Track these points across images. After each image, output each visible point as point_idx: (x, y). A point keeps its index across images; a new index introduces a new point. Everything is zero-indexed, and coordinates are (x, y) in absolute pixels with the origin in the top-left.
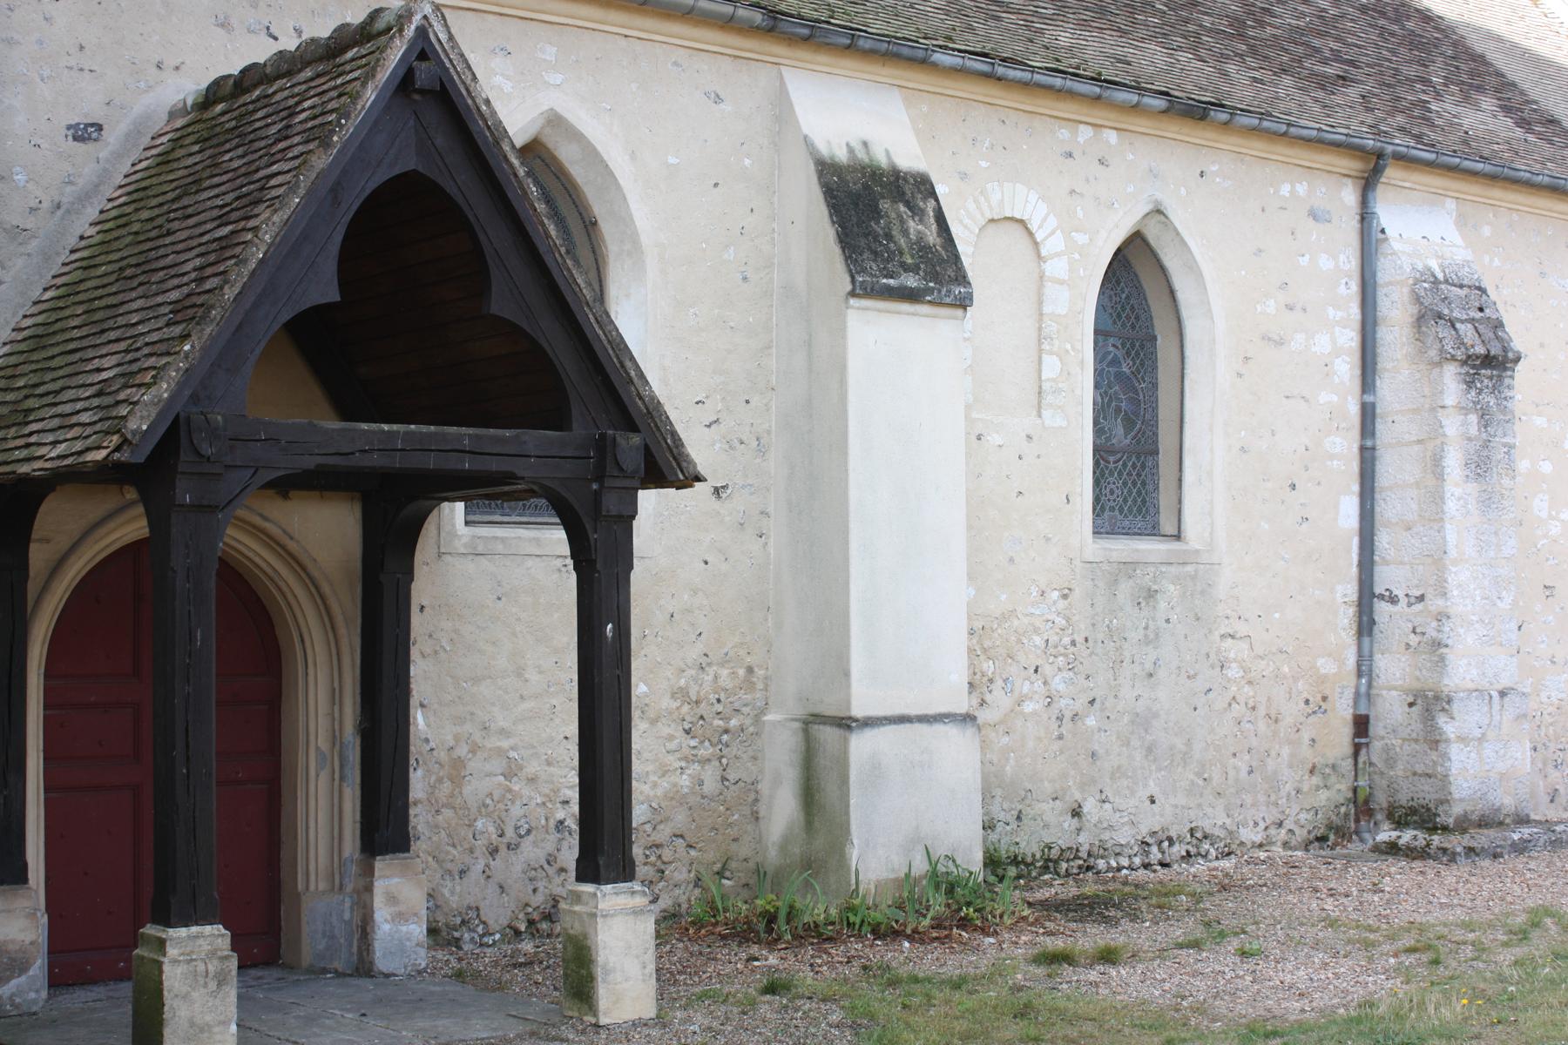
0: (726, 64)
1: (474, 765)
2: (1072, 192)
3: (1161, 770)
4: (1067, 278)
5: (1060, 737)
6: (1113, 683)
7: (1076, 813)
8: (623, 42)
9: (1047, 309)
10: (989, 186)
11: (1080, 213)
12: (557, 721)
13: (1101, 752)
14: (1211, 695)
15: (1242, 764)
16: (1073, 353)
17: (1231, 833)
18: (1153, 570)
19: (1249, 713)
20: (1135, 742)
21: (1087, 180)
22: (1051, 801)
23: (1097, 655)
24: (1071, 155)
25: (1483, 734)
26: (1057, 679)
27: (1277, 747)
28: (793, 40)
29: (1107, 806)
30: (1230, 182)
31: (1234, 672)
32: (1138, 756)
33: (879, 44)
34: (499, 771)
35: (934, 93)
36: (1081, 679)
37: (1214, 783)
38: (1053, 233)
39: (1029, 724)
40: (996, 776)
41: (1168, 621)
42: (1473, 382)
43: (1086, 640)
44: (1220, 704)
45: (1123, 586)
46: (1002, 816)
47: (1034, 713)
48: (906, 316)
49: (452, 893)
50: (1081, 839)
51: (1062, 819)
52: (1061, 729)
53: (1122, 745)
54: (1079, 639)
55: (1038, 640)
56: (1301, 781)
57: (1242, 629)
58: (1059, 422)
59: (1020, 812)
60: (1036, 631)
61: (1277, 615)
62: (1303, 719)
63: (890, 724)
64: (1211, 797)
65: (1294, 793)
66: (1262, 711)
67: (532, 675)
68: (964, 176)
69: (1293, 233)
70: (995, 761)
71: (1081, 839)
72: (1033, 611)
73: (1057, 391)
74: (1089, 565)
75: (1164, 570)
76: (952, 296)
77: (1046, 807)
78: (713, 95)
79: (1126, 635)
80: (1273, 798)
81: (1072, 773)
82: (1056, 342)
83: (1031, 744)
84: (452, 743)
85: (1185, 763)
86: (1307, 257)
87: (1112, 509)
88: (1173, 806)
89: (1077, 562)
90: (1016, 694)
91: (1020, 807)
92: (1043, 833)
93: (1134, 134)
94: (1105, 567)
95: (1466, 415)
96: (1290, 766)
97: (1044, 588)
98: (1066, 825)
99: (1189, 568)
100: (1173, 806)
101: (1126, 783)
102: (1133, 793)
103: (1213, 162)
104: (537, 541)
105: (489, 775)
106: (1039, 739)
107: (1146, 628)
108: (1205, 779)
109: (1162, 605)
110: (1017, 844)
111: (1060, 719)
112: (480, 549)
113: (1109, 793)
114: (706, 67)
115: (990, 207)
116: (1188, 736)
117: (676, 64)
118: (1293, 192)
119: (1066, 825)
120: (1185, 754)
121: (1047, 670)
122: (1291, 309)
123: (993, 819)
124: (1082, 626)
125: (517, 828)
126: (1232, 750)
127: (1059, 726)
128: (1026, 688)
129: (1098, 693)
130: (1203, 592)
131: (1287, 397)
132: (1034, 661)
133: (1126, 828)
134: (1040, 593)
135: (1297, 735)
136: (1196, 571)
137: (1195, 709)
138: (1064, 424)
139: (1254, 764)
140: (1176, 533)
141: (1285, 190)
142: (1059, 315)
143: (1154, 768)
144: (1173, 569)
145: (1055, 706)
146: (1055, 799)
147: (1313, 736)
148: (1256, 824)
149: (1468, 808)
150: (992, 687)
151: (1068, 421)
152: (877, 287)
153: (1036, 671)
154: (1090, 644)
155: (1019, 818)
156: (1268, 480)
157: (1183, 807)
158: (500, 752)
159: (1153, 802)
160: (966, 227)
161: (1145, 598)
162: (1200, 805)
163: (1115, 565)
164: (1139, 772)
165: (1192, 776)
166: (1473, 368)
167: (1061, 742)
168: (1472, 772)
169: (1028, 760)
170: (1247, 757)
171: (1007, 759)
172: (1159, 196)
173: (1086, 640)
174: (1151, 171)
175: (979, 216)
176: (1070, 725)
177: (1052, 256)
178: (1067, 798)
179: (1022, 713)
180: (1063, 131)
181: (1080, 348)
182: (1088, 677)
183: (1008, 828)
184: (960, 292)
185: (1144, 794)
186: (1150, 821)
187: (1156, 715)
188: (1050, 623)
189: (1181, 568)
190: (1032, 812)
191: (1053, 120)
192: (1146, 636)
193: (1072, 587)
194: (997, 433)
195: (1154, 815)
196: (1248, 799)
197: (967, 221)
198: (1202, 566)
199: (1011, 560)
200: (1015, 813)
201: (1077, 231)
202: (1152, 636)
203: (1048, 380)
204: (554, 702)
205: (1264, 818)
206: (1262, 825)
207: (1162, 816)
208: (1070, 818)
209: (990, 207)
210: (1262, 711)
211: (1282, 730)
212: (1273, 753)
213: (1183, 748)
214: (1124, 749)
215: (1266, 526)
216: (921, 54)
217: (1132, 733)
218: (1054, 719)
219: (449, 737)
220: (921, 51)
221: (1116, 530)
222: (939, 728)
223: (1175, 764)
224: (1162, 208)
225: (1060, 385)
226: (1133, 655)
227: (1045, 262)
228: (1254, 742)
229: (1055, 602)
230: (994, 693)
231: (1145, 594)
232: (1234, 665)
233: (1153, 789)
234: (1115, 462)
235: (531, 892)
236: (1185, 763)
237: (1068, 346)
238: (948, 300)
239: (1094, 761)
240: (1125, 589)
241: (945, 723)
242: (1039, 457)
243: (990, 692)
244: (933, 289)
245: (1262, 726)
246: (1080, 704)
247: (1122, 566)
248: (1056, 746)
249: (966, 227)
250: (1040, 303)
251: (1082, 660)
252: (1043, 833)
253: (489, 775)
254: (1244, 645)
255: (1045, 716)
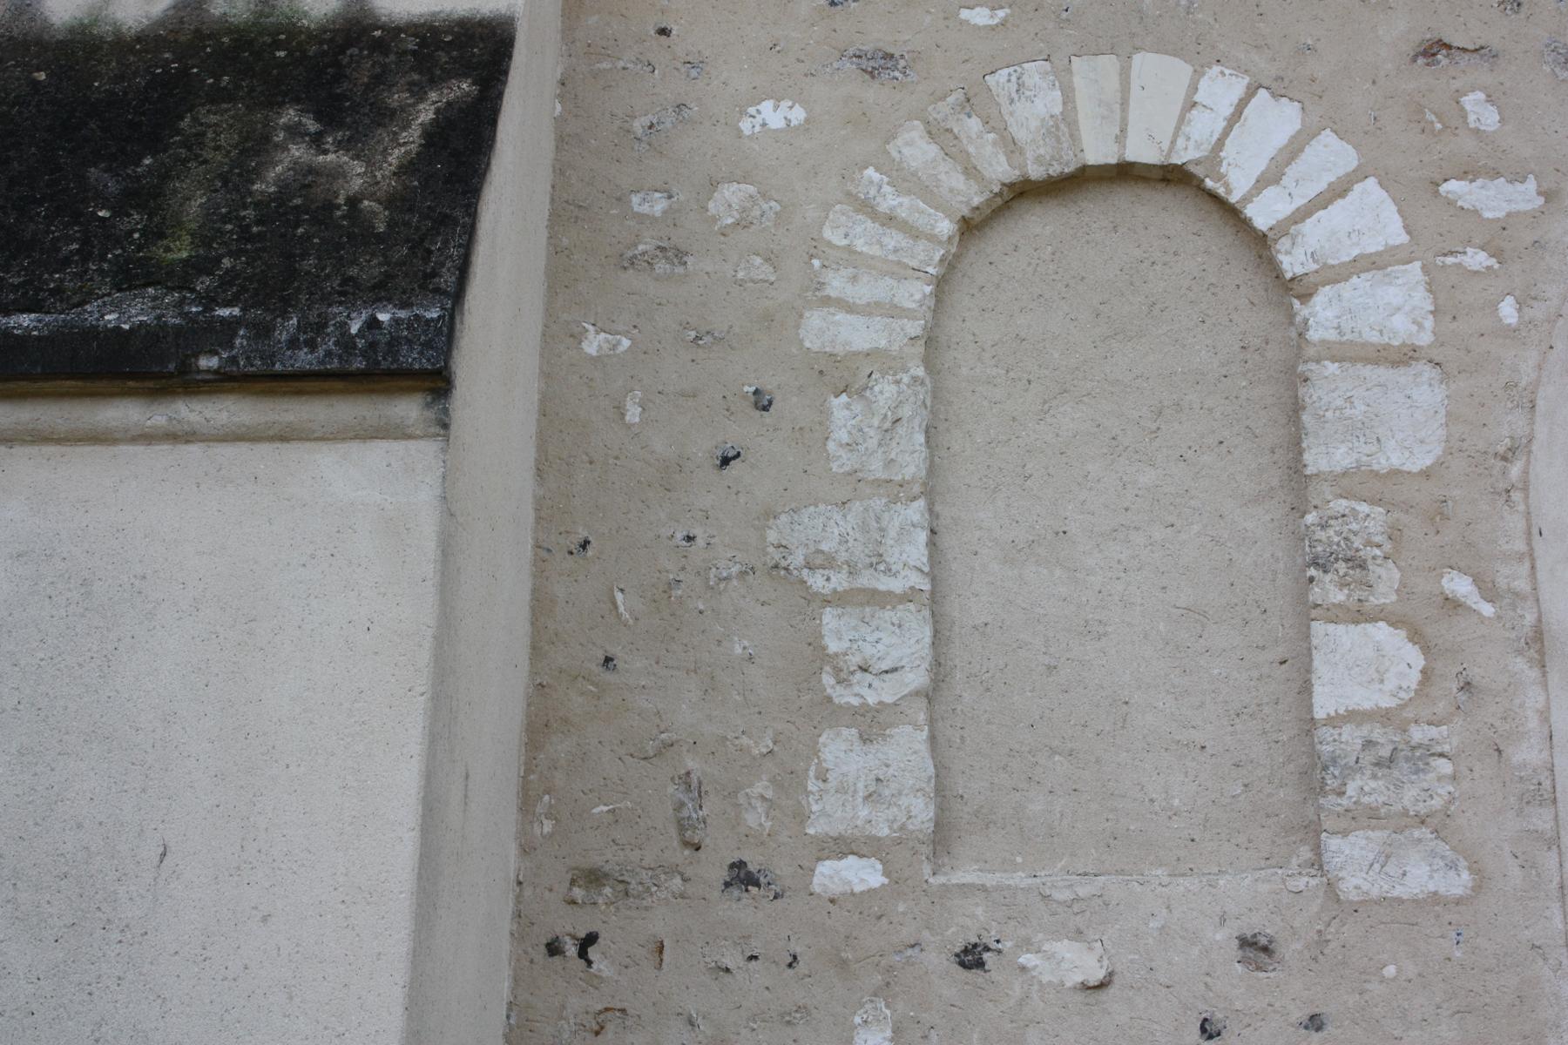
4: (1425, 339)
9: (1316, 459)
10: (1000, 80)
16: (1487, 610)
48: (139, 449)
138: (1458, 883)
151: (1476, 869)
160: (889, 220)
181: (1522, 585)
184: (373, 323)
194: (1079, 934)
201: (1467, 174)
225: (1418, 734)
227: (1305, 297)
237: (1460, 586)
238: (304, 359)
244: (231, 325)
249: (889, 220)
250: (1296, 446)
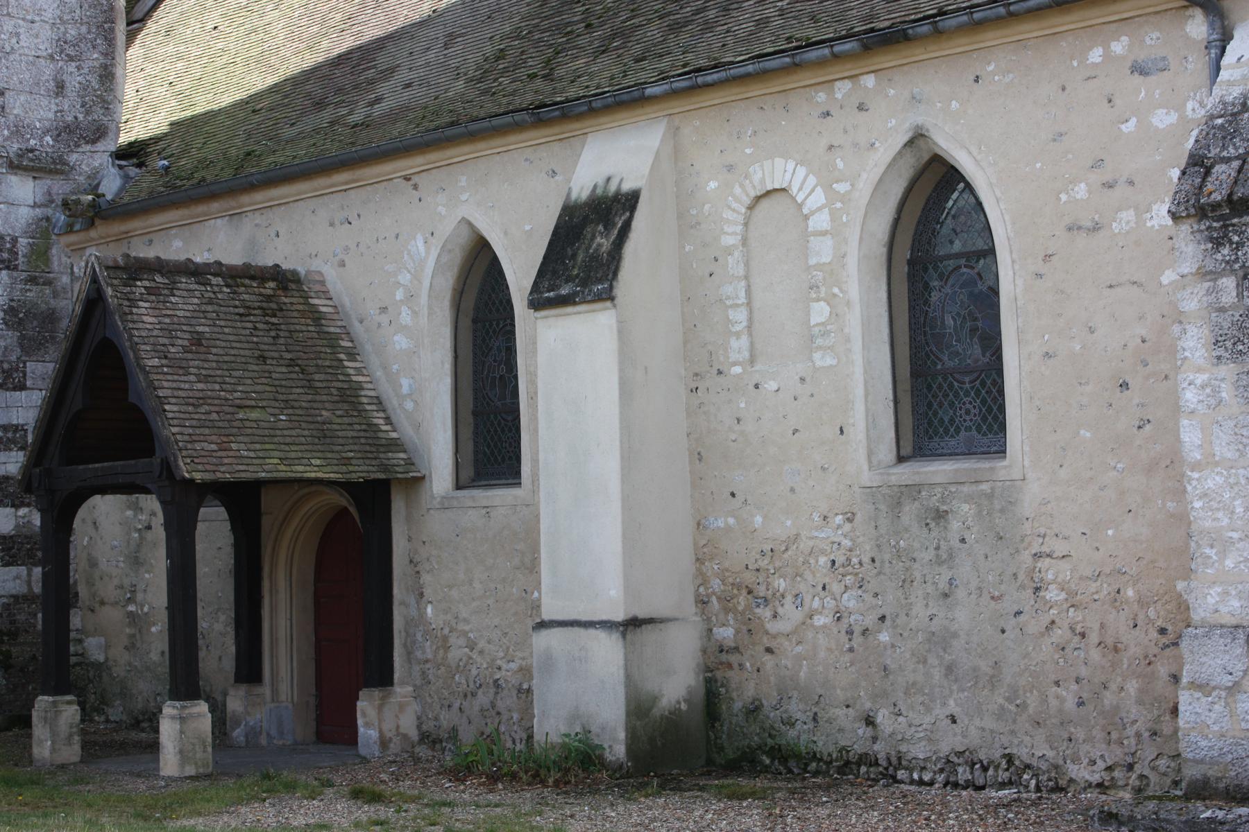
0: (556, 146)
1: (453, 640)
2: (831, 147)
3: (963, 691)
4: (829, 229)
5: (851, 650)
6: (903, 602)
7: (870, 722)
8: (498, 158)
11: (840, 164)
12: (491, 615)
13: (893, 666)
14: (1022, 618)
15: (1069, 695)
17: (1056, 767)
18: (940, 490)
19: (1077, 639)
20: (932, 660)
21: (846, 132)
22: (844, 708)
23: (884, 574)
24: (828, 114)
25: (1236, 683)
26: (845, 596)
27: (1119, 679)
28: (580, 117)
29: (901, 719)
30: (1011, 76)
31: (1052, 594)
32: (937, 674)
33: (605, 100)
34: (464, 645)
35: (695, 109)
36: (868, 597)
37: (1031, 710)
38: (813, 190)
39: (820, 636)
40: (791, 680)
41: (963, 541)
42: (1226, 235)
43: (873, 560)
44: (1034, 627)
45: (907, 508)
46: (799, 715)
47: (824, 626)
49: (445, 719)
50: (876, 747)
51: (857, 725)
52: (853, 643)
53: (918, 662)
54: (866, 560)
55: (823, 560)
56: (1157, 720)
57: (1060, 548)
58: (830, 361)
59: (816, 714)
60: (823, 552)
61: (1110, 532)
62: (1156, 650)
63: (558, 626)
64: (1027, 725)
65: (1146, 734)
66: (1094, 638)
67: (477, 585)
68: (730, 168)
69: (1110, 101)
70: (790, 666)
71: (876, 747)
72: (816, 534)
73: (825, 334)
74: (868, 490)
75: (954, 490)
76: (592, 294)
77: (840, 712)
78: (551, 172)
79: (915, 555)
80: (1114, 736)
81: (864, 684)
82: (823, 289)
83: (822, 654)
84: (442, 626)
85: (993, 685)
86: (1133, 121)
87: (968, 429)
88: (978, 728)
89: (856, 488)
90: (806, 607)
91: (814, 709)
92: (839, 736)
93: (883, 71)
94: (885, 491)
95: (1215, 280)
96: (1140, 702)
97: (825, 513)
98: (860, 732)
99: (985, 487)
100: (978, 728)
101: (921, 699)
102: (929, 710)
103: (989, 64)
104: (473, 498)
105: (460, 647)
106: (830, 650)
107: (937, 548)
108: (1017, 706)
109: (955, 525)
110: (815, 742)
111: (850, 632)
112: (446, 506)
113: (902, 706)
114: (545, 154)
115: (754, 187)
116: (994, 660)
117: (526, 160)
118: (1107, 55)
119: (860, 732)
120: (993, 676)
121: (836, 587)
122: (1111, 187)
123: (791, 717)
124: (868, 547)
125: (475, 682)
126: (1053, 677)
127: (850, 640)
128: (816, 603)
129: (885, 610)
130: (1002, 511)
131: (1111, 286)
132: (820, 580)
133: (923, 743)
134: (822, 517)
135: (1149, 669)
136: (992, 488)
137: (1003, 631)
138: (834, 362)
139: (1085, 695)
140: (461, 483)
141: (1096, 55)
142: (824, 264)
143: (955, 687)
144: (965, 489)
145: (845, 621)
146: (848, 706)
147: (1173, 671)
148: (1093, 763)
149: (1210, 773)
150: (784, 601)
152: (541, 301)
153: (824, 588)
154: (877, 564)
155: (815, 719)
156: (1087, 383)
157: (992, 731)
158: (465, 633)
159: (954, 722)
161: (933, 519)
162: (1012, 732)
163: (896, 489)
164: (937, 690)
165: (1001, 701)
166: (1217, 221)
167: (852, 654)
168: (1216, 728)
169: (821, 668)
170: (1074, 687)
171: (801, 666)
172: (920, 117)
173: (873, 560)
174: (914, 98)
175: (745, 198)
176: (861, 639)
177: (813, 213)
178: (858, 707)
179: (812, 626)
180: (820, 94)
182: (876, 595)
183: (805, 727)
184: (598, 289)
185: (940, 712)
186: (950, 742)
187: (955, 635)
188: (836, 544)
189: (974, 487)
190: (827, 716)
191: (808, 89)
192: (937, 556)
193: (854, 511)
194: (774, 380)
195: (955, 735)
196: (1080, 734)
197: (734, 205)
198: (1000, 484)
199: (792, 490)
200: (811, 714)
201: (837, 182)
202: (945, 556)
203: (818, 325)
204: (489, 602)
205: (1102, 756)
206: (1101, 765)
207: (964, 736)
208: (864, 726)
209: (754, 187)
210: (1094, 638)
211: (1125, 661)
212: (1113, 687)
213: (990, 671)
214: (921, 666)
215: (1088, 435)
216: (636, 94)
217: (929, 651)
218: (843, 632)
219: (441, 622)
220: (636, 92)
221: (974, 450)
222: (592, 631)
223: (980, 685)
224: (924, 132)
225: (828, 328)
226: (925, 575)
228: (1084, 672)
229: (839, 527)
230: (786, 606)
231: (933, 515)
232: (1052, 587)
233: (952, 707)
234: (971, 382)
235: (484, 725)
236: (993, 685)
237: (836, 290)
238: (589, 298)
239: (887, 676)
240: (910, 512)
241: (596, 628)
242: (812, 395)
243: (782, 605)
244: (579, 291)
245: (1095, 655)
246: (870, 620)
247: (903, 489)
248: (847, 657)
249: (734, 210)
251: (869, 579)
252: (839, 736)
253: (460, 647)
254: (1065, 565)
255: (835, 630)
